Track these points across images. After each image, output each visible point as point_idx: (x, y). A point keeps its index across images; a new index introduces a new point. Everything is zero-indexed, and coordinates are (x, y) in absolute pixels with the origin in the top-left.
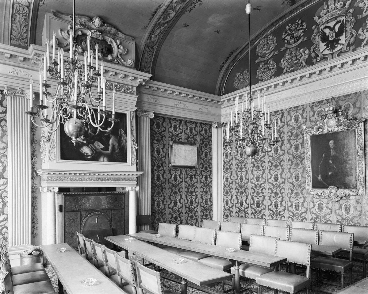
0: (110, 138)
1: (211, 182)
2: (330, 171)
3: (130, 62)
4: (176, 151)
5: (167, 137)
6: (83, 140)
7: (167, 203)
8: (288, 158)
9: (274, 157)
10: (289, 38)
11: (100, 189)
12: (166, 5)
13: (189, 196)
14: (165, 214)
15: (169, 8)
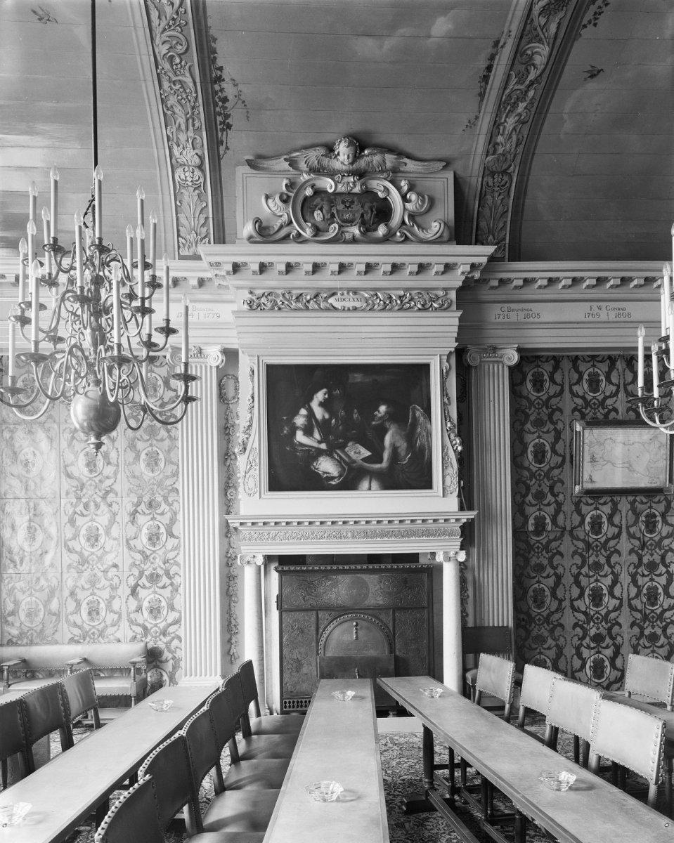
0: (385, 431)
4: (596, 449)
5: (567, 411)
6: (320, 442)
7: (567, 596)
11: (373, 558)
12: (513, 34)
13: (643, 575)
14: (562, 626)
15: (524, 41)
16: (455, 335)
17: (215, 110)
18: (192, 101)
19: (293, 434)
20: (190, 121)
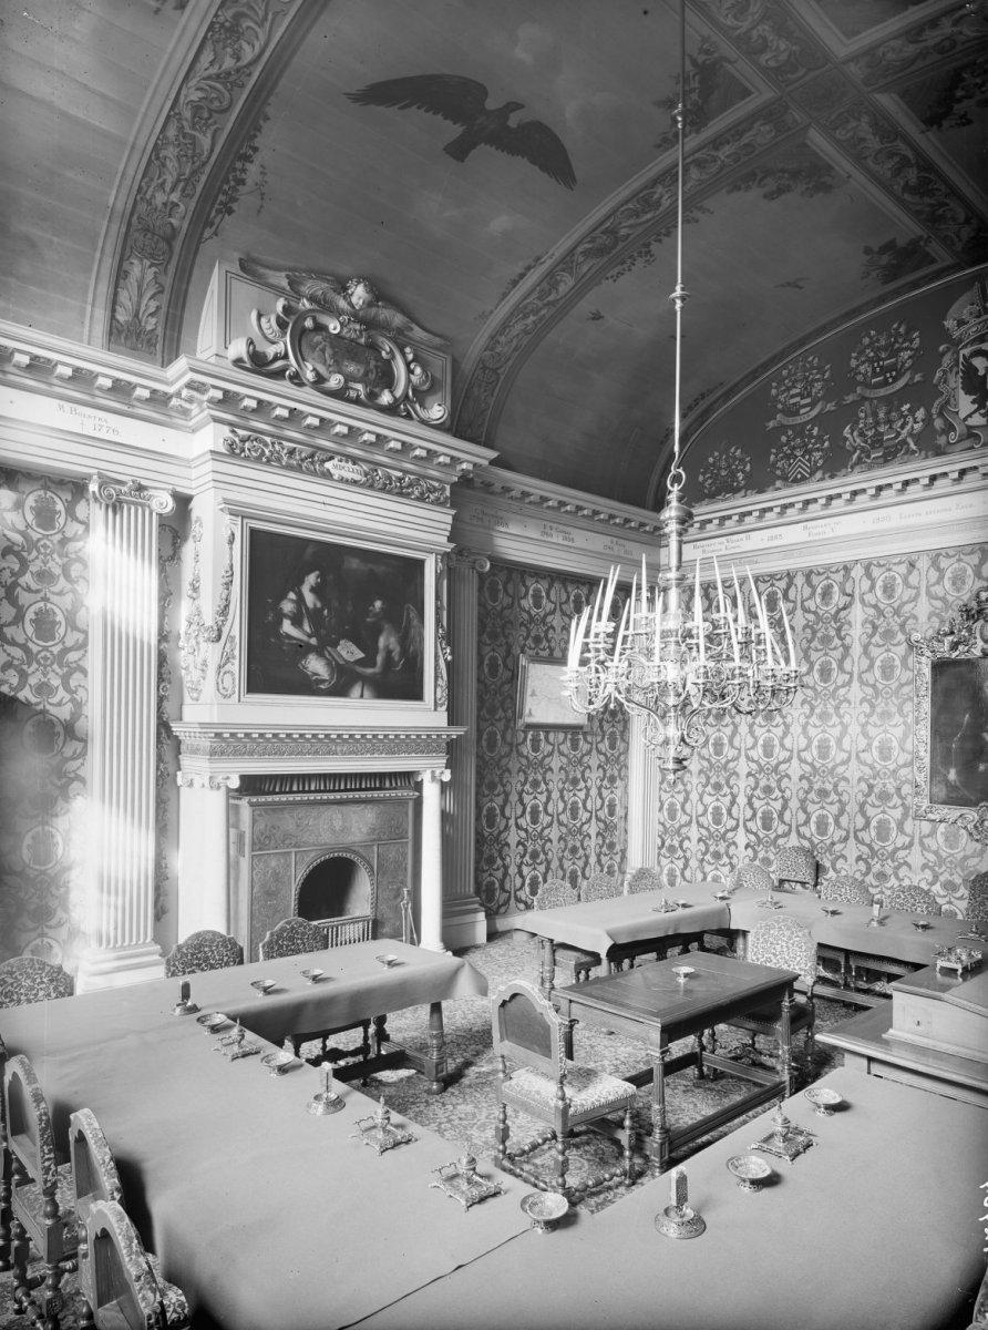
0: (379, 632)
1: (627, 750)
3: (437, 412)
6: (310, 636)
8: (862, 695)
9: (819, 689)
10: (869, 369)
15: (561, 266)
18: (197, 164)
19: (281, 623)
20: (182, 185)
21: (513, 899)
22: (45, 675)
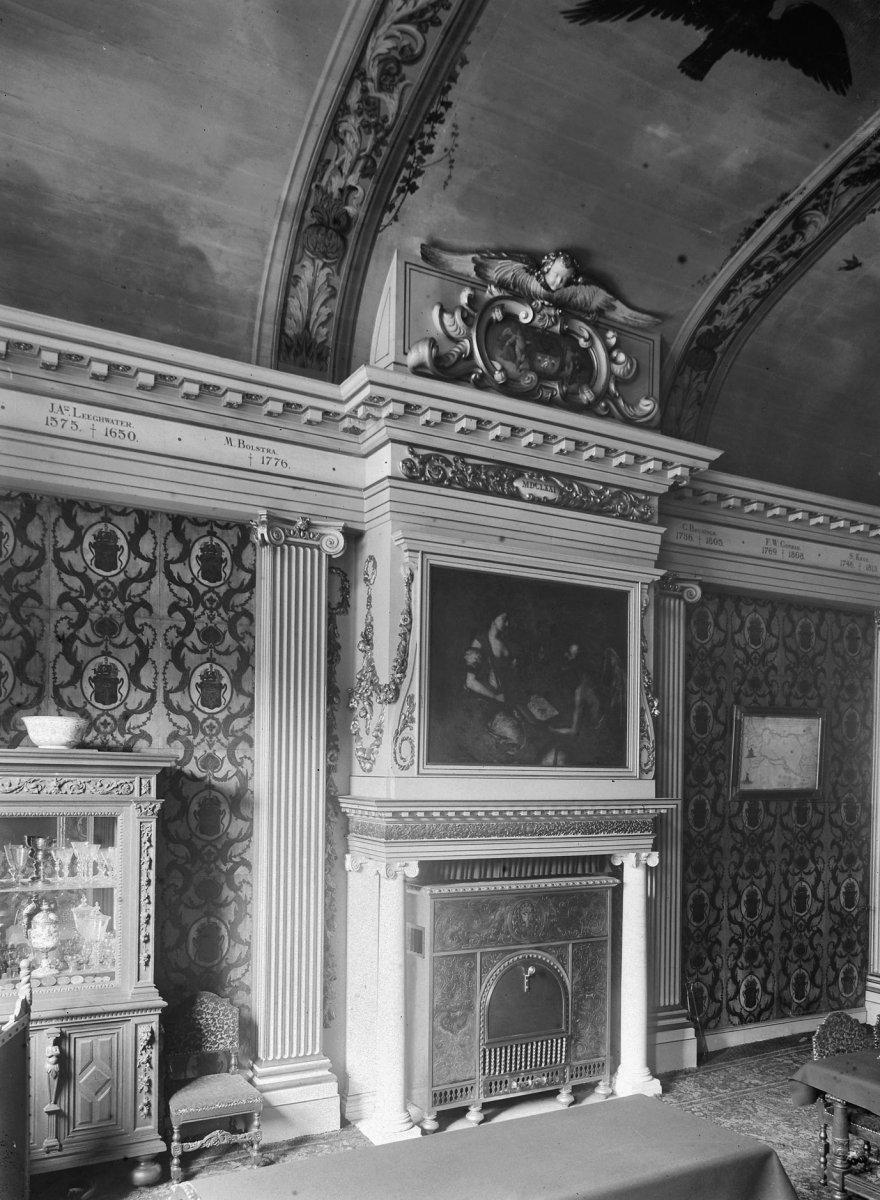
2: (578, 655)
6: (496, 692)
15: (814, 201)
16: (655, 557)
17: (406, 158)
21: (724, 1011)
22: (210, 746)
